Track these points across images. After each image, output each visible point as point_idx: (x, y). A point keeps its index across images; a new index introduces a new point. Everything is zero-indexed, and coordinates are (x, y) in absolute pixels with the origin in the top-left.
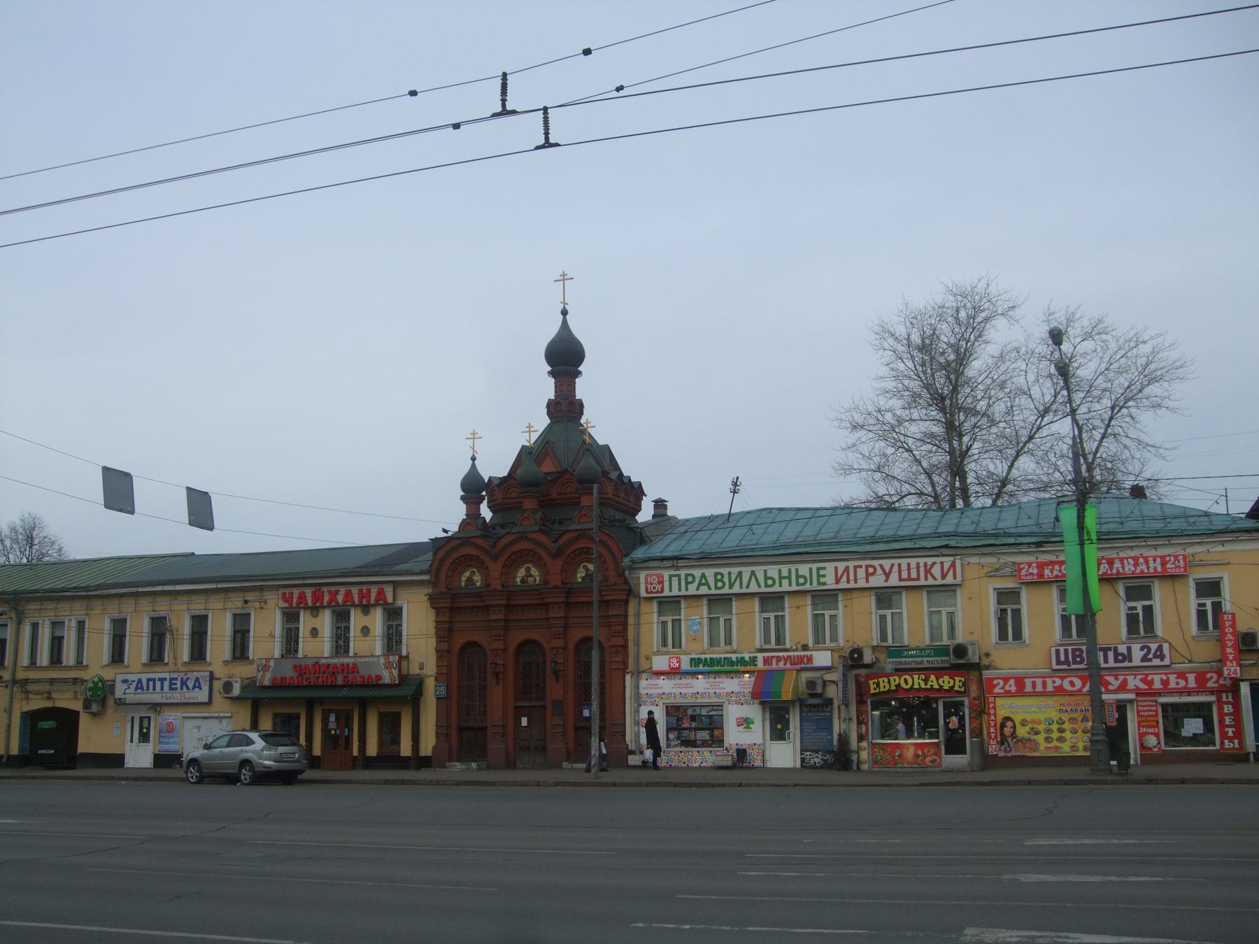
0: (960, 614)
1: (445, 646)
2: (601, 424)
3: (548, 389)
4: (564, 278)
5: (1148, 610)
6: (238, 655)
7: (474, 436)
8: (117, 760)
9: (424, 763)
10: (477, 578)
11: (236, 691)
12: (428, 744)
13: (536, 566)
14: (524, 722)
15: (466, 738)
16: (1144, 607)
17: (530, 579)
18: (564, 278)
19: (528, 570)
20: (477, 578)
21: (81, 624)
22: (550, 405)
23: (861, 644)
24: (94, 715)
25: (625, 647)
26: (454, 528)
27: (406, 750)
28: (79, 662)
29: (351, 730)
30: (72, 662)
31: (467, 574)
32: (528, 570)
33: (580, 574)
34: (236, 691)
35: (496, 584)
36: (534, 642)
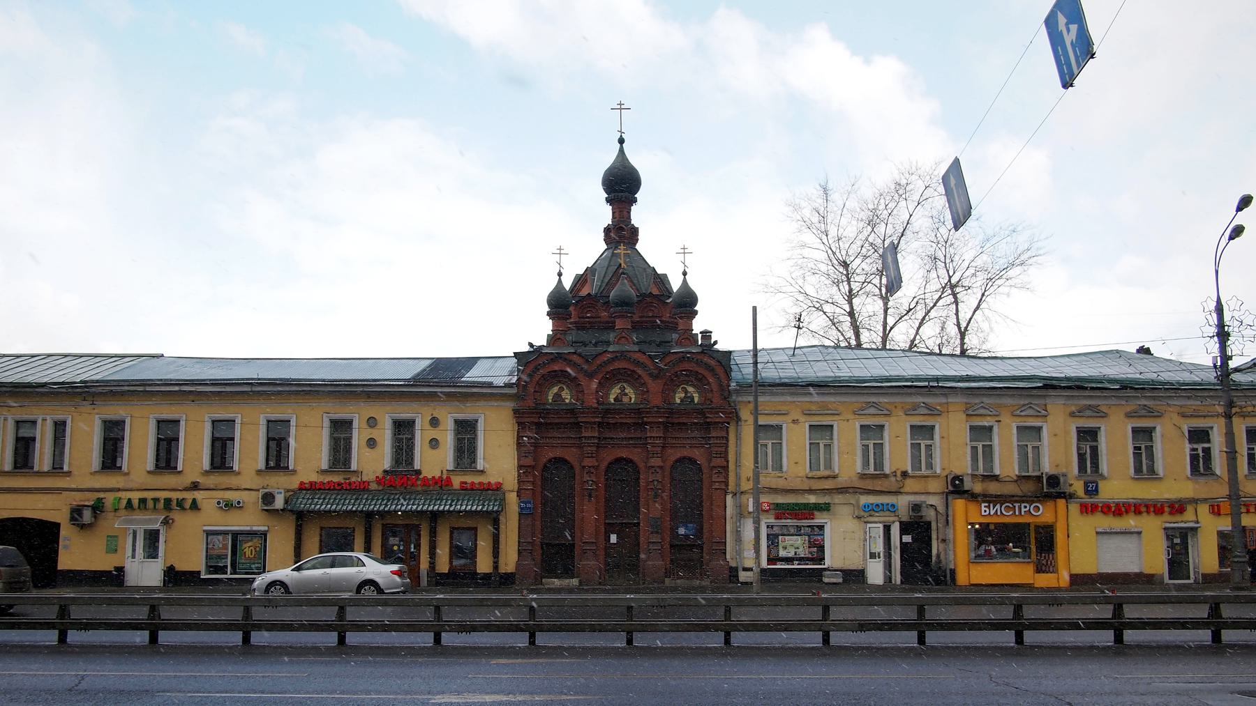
0: (1046, 449)
1: (529, 461)
2: (659, 249)
3: (605, 215)
4: (621, 107)
5: (1207, 451)
6: (272, 464)
7: (684, 251)
8: (116, 577)
9: (506, 581)
10: (567, 396)
11: (279, 503)
12: (509, 561)
13: (633, 386)
14: (614, 538)
15: (553, 555)
16: (1204, 450)
17: (625, 400)
18: (621, 107)
19: (623, 389)
20: (567, 396)
21: (60, 426)
22: (607, 231)
23: (958, 472)
24: (83, 527)
25: (726, 468)
26: (541, 340)
27: (484, 565)
28: (57, 468)
29: (418, 546)
30: (46, 467)
31: (555, 389)
32: (623, 389)
33: (679, 397)
34: (279, 503)
35: (656, 400)
36: (629, 461)
